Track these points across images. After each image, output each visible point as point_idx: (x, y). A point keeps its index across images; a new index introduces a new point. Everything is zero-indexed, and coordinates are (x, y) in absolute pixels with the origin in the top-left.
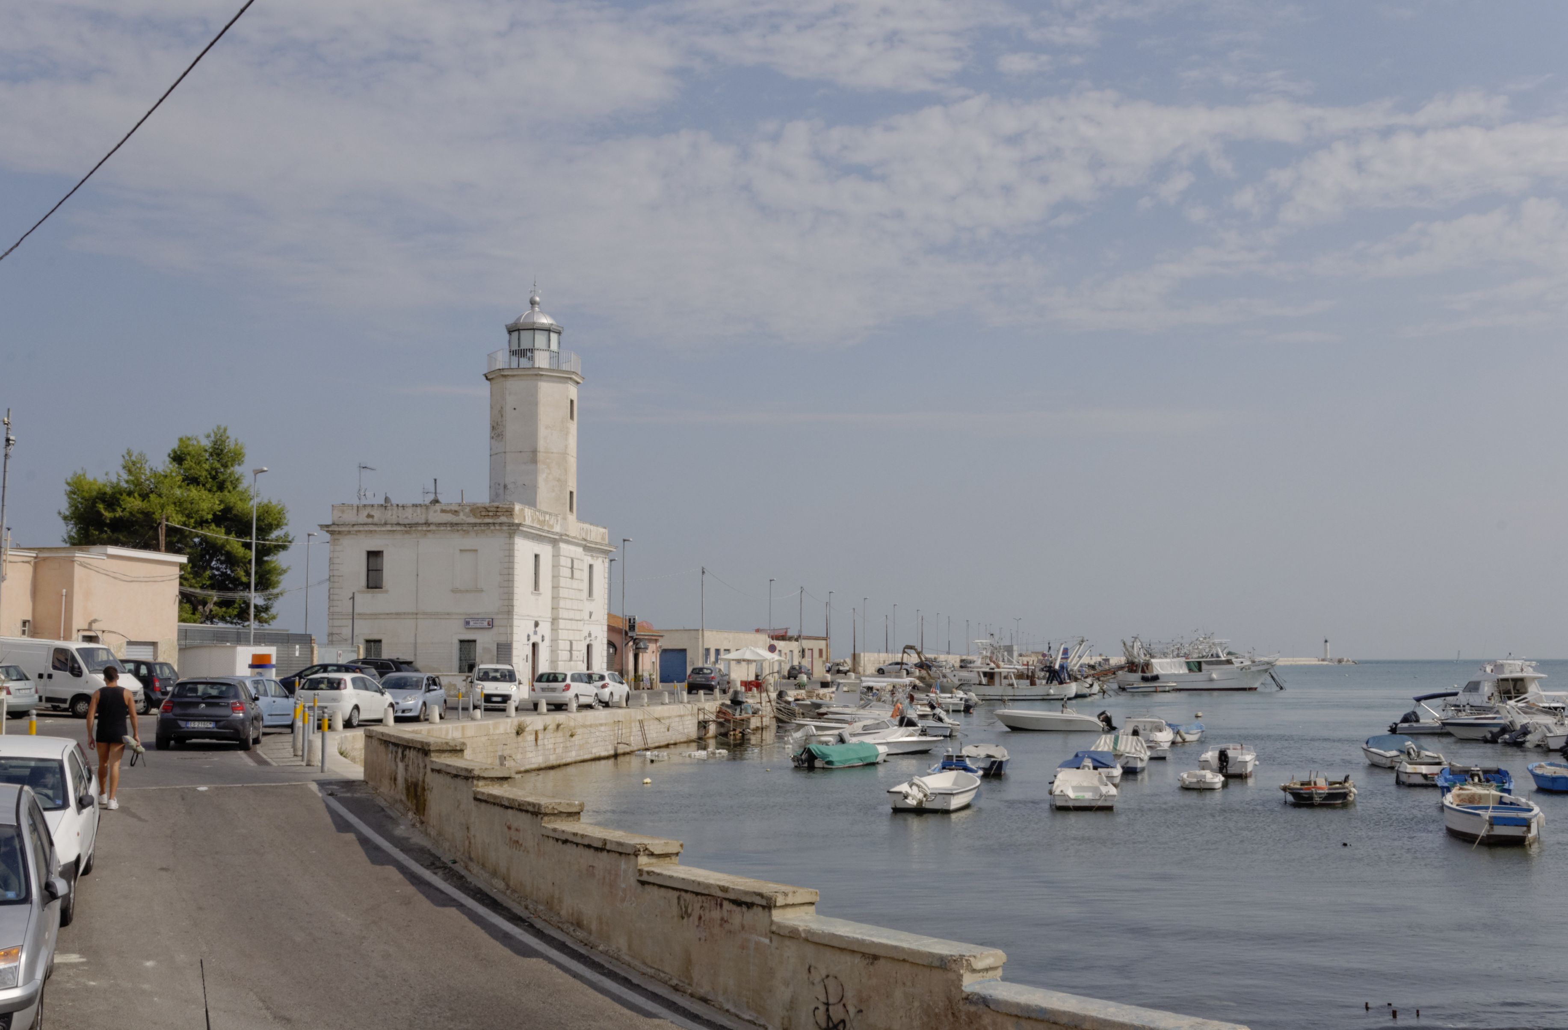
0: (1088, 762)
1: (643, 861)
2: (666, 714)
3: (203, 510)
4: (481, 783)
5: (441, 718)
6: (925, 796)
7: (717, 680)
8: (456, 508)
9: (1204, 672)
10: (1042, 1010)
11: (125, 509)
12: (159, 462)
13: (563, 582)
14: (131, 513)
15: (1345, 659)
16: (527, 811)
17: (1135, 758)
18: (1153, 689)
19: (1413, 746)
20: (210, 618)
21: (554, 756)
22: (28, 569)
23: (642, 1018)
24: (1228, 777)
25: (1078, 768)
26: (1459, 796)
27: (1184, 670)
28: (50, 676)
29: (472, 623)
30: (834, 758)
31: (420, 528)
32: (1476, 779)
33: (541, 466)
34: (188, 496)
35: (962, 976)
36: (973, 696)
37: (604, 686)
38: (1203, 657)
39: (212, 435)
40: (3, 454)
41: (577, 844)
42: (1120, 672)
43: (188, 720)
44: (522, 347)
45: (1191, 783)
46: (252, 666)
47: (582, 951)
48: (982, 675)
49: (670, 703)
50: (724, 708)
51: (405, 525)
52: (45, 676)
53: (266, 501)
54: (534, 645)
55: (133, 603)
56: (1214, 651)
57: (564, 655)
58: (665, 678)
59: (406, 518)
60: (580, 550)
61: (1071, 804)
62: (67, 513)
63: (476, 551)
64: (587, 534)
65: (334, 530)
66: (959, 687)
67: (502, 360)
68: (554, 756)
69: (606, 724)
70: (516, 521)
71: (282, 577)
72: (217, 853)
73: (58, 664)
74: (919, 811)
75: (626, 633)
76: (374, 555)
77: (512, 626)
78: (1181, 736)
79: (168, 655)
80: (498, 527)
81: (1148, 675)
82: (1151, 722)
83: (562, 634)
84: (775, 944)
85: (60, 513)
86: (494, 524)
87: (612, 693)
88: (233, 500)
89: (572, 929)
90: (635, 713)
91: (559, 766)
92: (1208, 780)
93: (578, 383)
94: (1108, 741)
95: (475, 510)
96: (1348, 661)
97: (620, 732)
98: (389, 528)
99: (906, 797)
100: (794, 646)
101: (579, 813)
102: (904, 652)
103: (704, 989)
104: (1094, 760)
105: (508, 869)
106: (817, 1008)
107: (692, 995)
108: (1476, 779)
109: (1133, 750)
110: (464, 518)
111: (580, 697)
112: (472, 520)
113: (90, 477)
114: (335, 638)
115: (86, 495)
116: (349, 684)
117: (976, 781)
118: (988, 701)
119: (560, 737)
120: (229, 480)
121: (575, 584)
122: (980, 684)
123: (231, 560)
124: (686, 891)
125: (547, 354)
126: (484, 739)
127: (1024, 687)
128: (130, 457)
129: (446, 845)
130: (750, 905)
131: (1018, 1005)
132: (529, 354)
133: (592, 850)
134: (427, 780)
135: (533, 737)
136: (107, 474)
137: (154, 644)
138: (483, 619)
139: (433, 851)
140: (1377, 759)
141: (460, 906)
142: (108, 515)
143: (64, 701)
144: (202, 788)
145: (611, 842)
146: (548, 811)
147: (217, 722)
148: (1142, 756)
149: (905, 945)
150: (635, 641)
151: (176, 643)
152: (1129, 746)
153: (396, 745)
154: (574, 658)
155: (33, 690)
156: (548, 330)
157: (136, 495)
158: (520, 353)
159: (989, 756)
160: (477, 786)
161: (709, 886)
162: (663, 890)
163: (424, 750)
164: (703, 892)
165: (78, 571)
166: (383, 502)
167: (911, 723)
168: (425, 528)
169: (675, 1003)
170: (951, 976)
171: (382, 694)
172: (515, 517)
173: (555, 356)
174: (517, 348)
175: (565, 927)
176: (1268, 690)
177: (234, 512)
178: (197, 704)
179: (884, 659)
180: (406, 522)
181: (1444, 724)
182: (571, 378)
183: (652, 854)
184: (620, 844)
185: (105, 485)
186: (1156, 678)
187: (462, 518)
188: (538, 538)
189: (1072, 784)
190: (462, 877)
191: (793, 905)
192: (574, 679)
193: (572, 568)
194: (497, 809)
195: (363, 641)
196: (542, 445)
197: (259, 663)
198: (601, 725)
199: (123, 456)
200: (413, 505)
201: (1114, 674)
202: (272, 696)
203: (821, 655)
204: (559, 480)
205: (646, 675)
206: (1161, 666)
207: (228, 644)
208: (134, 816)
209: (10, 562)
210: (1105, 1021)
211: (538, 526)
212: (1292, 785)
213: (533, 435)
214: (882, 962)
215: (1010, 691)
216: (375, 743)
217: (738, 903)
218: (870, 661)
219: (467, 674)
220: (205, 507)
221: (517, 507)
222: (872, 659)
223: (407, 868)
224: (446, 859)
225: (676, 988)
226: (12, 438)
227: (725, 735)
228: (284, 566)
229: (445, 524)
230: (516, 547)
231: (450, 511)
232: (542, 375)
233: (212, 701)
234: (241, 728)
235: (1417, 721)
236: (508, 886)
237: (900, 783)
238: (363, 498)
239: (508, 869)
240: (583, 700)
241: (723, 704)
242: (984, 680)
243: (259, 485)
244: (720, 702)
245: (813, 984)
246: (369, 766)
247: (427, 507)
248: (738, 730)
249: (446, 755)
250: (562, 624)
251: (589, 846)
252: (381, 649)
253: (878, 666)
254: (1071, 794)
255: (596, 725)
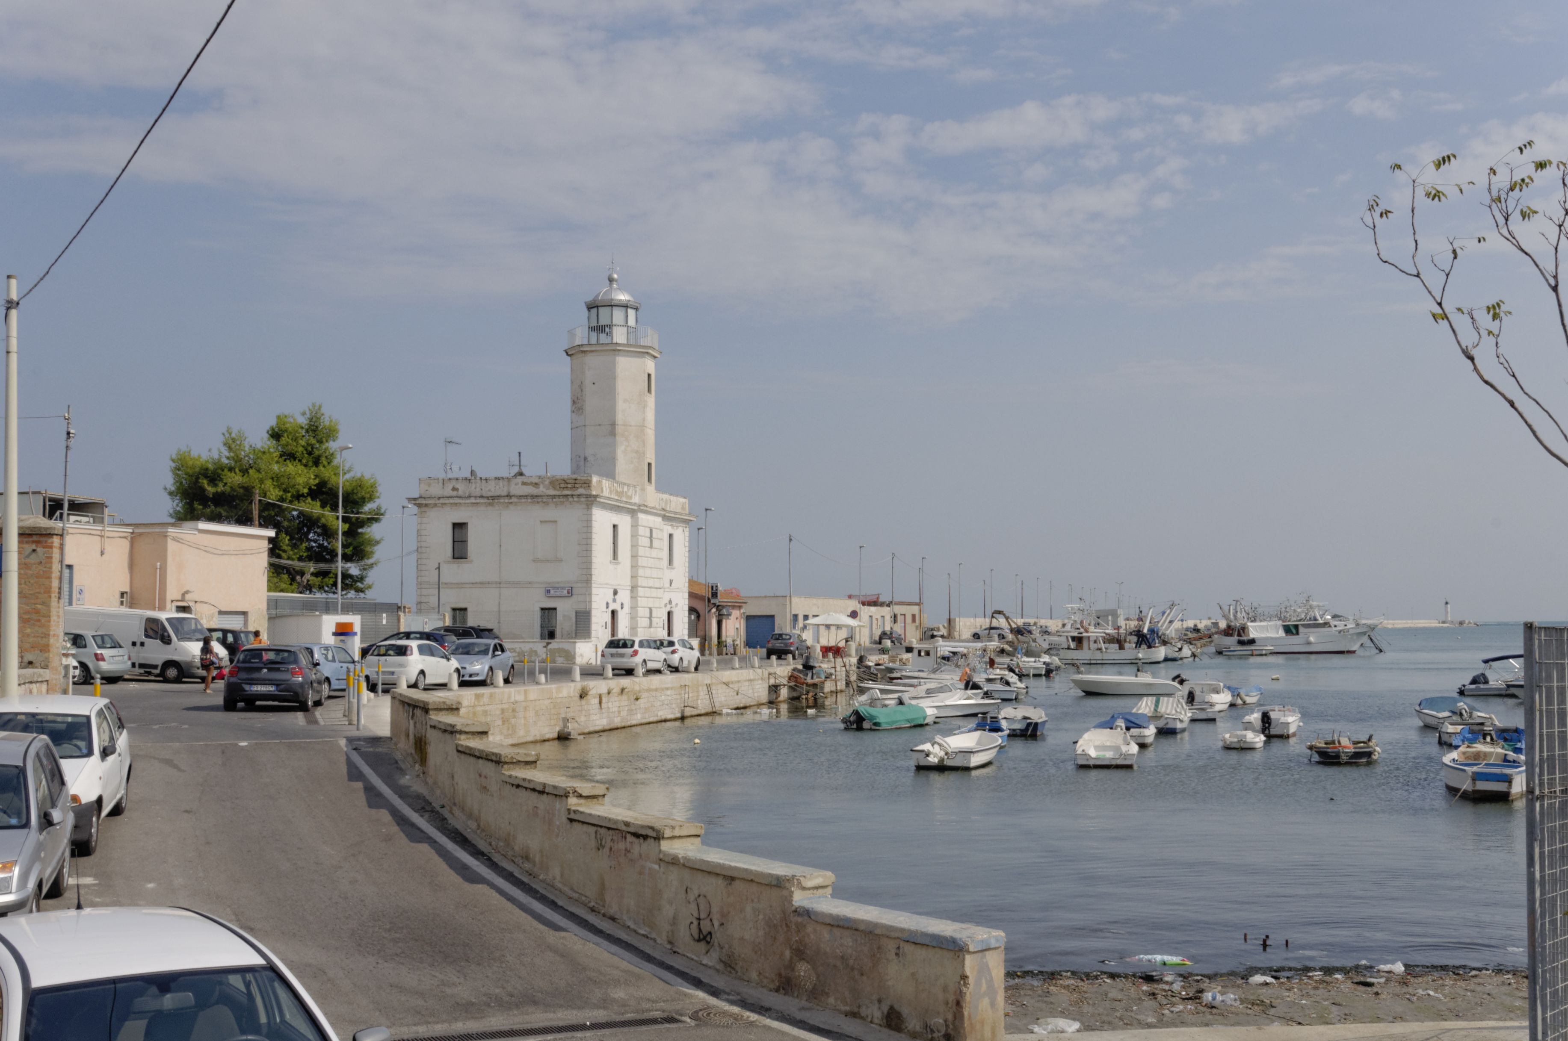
0: (1121, 723)
1: (572, 801)
2: (735, 679)
3: (299, 484)
4: (463, 737)
5: (507, 681)
6: (947, 754)
7: (796, 645)
8: (537, 481)
9: (1301, 635)
10: (847, 919)
11: (226, 484)
12: (257, 438)
13: (641, 551)
14: (231, 487)
15: (1467, 622)
16: (492, 761)
17: (1174, 719)
18: (1249, 653)
19: (1465, 707)
20: (309, 588)
21: (619, 719)
22: (126, 544)
23: (552, 932)
24: (1270, 738)
25: (1111, 728)
26: (1464, 753)
27: (1281, 633)
28: (142, 644)
29: (552, 592)
30: (881, 719)
31: (502, 501)
32: (1488, 739)
33: (619, 439)
34: (285, 471)
35: (793, 892)
36: (1056, 661)
37: (673, 652)
38: (1300, 620)
39: (308, 413)
40: (64, 444)
41: (526, 788)
42: (1216, 636)
43: (251, 684)
44: (601, 323)
45: (1232, 742)
46: (336, 634)
47: (525, 879)
48: (1070, 640)
49: (741, 668)
50: (796, 673)
51: (488, 498)
52: (138, 644)
53: (359, 475)
54: (613, 613)
55: (225, 576)
56: (1311, 614)
57: (643, 622)
58: (750, 643)
59: (489, 490)
60: (660, 519)
61: (1091, 763)
62: (173, 489)
63: (556, 521)
64: (666, 503)
65: (421, 503)
66: (1048, 652)
67: (581, 336)
68: (619, 719)
69: (672, 688)
70: (594, 493)
71: (376, 548)
72: (237, 798)
73: (151, 633)
74: (941, 768)
75: (709, 600)
76: (459, 527)
77: (590, 594)
78: (1241, 699)
79: (258, 622)
80: (576, 499)
81: (1245, 638)
82: (1209, 684)
83: (642, 602)
84: (662, 869)
85: (165, 489)
86: (572, 495)
87: (681, 659)
88: (327, 475)
89: (521, 861)
90: (703, 678)
91: (624, 727)
92: (1248, 740)
93: (655, 357)
94: (1149, 703)
95: (555, 483)
96: (1469, 623)
97: (686, 696)
98: (473, 500)
99: (928, 755)
100: (886, 611)
101: (535, 762)
102: (993, 617)
103: (613, 911)
104: (1127, 720)
105: (479, 811)
106: (692, 923)
107: (604, 915)
108: (1488, 739)
109: (1174, 712)
110: (544, 490)
111: (648, 663)
112: (552, 492)
113: (194, 454)
114: (423, 606)
115: (190, 472)
116: (415, 650)
117: (998, 741)
118: (1074, 665)
119: (624, 701)
120: (324, 455)
121: (654, 553)
122: (1069, 648)
123: (328, 533)
124: (601, 827)
125: (625, 329)
126: (547, 702)
127: (1113, 651)
128: (230, 434)
129: (438, 792)
130: (645, 837)
131: (831, 915)
132: (607, 330)
133: (536, 793)
134: (428, 735)
135: (597, 701)
136: (210, 450)
137: (244, 614)
138: (563, 588)
139: (428, 797)
140: (1430, 721)
141: (432, 842)
142: (210, 490)
143: (155, 667)
144: (243, 744)
145: (549, 785)
146: (508, 760)
147: (277, 685)
148: (1182, 717)
149: (753, 868)
150: (719, 608)
151: (265, 612)
152: (1170, 708)
153: (409, 705)
154: (654, 624)
155: (126, 657)
156: (625, 306)
157: (237, 470)
158: (600, 329)
159: (1025, 718)
160: (460, 740)
161: (616, 822)
162: (585, 826)
163: (426, 709)
164: (613, 826)
165: (171, 545)
166: (468, 475)
167: (976, 687)
168: (507, 501)
169: (586, 921)
170: (785, 893)
171: (448, 659)
172: (593, 488)
173: (631, 331)
174: (595, 324)
175: (516, 860)
176: (1367, 653)
177: (329, 486)
178: (259, 669)
179: (981, 623)
180: (490, 494)
181: (1509, 686)
182: (647, 353)
183: (580, 796)
184: (555, 787)
185: (207, 462)
186: (1252, 642)
187: (542, 490)
188: (616, 509)
189: (1095, 743)
190: (445, 819)
191: (680, 837)
192: (641, 644)
193: (651, 537)
194: (472, 759)
195: (450, 610)
196: (620, 418)
197: (343, 631)
198: (667, 689)
199: (223, 434)
200: (496, 478)
201: (1210, 637)
202: (340, 662)
203: (914, 620)
204: (637, 452)
205: (729, 641)
206: (1254, 631)
207: (317, 613)
208: (176, 767)
209: (108, 537)
210: (891, 927)
211: (616, 498)
212: (1318, 745)
213: (612, 409)
214: (737, 882)
215: (1098, 656)
216: (397, 703)
217: (636, 835)
218: (966, 626)
219: (547, 641)
220: (301, 482)
221: (595, 479)
222: (968, 624)
223: (399, 811)
224: (436, 805)
225: (593, 910)
226: (72, 431)
227: (798, 698)
228: (377, 537)
229: (526, 496)
230: (594, 518)
231: (531, 484)
232: (619, 350)
233: (273, 666)
234: (300, 691)
235: (1486, 682)
236: (479, 826)
237: (923, 743)
238: (449, 471)
239: (479, 811)
240: (651, 665)
241: (794, 670)
242: (1073, 645)
243: (354, 459)
244: (792, 667)
245: (689, 902)
246: (394, 724)
247: (509, 480)
248: (811, 694)
249: (443, 712)
250: (641, 592)
251: (534, 790)
252: (466, 616)
253: (973, 631)
254: (1093, 753)
255: (662, 690)
